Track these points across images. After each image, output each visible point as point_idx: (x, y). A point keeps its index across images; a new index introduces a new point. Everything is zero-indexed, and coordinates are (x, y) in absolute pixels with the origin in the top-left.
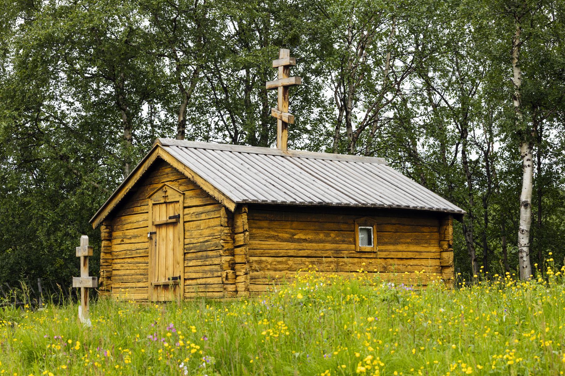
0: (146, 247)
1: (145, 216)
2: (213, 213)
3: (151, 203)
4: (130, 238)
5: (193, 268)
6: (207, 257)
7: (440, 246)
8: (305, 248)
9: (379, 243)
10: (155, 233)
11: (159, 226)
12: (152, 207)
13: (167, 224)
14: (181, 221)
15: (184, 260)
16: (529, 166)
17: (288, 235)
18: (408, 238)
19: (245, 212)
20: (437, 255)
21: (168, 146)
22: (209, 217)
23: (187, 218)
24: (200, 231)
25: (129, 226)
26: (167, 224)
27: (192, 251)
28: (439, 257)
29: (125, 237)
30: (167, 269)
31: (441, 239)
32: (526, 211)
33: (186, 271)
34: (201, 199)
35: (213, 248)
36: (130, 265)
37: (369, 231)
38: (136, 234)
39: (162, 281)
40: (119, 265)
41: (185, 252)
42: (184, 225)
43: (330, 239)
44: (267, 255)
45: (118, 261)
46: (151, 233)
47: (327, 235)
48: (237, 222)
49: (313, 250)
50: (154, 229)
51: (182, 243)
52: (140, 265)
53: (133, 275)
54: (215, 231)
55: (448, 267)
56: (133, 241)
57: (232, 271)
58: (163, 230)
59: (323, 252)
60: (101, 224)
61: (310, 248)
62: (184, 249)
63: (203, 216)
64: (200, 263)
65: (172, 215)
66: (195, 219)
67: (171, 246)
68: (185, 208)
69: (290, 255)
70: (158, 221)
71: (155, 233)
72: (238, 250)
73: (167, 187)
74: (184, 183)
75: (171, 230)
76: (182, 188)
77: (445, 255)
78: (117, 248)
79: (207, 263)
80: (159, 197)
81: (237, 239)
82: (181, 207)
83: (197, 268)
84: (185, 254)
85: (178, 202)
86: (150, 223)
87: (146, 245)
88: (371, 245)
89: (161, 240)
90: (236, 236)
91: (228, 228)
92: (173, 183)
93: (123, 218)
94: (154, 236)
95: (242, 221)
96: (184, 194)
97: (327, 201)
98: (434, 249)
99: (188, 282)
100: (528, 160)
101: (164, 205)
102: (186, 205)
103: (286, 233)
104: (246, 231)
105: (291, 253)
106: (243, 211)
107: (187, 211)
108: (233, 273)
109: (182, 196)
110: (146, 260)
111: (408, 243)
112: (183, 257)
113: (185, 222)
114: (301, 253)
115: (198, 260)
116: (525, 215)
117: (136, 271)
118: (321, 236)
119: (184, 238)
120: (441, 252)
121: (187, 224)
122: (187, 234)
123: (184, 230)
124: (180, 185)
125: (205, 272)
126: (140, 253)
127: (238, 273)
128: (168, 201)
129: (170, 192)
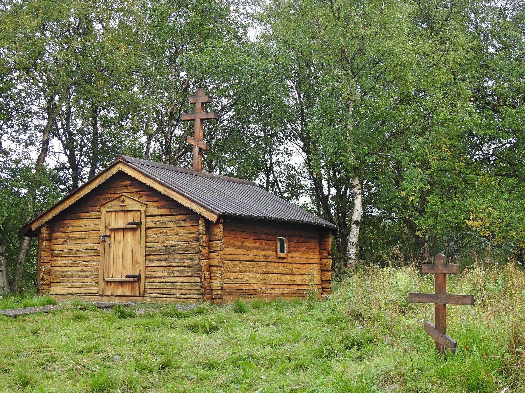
0: (96, 248)
1: (96, 221)
2: (183, 222)
3: (103, 210)
4: (76, 240)
5: (157, 268)
6: (174, 260)
7: (321, 254)
8: (249, 253)
9: (290, 251)
10: (109, 236)
11: (115, 230)
12: (106, 214)
13: (124, 230)
14: (143, 227)
15: (146, 261)
16: (360, 194)
17: (239, 243)
18: (303, 247)
19: (222, 223)
20: (317, 261)
21: (130, 163)
22: (178, 225)
23: (151, 225)
24: (166, 237)
25: (70, 229)
26: (124, 230)
27: (155, 253)
28: (319, 263)
29: (69, 238)
30: (124, 267)
31: (322, 248)
32: (357, 228)
33: (146, 271)
34: (167, 210)
35: (182, 252)
36: (74, 262)
37: (282, 242)
38: (83, 236)
39: (118, 278)
40: (60, 262)
41: (147, 254)
42: (146, 231)
43: (262, 246)
44: (228, 259)
45: (59, 259)
46: (105, 236)
47: (261, 244)
48: (213, 231)
49: (253, 255)
50: (108, 233)
51: (143, 246)
52: (87, 263)
53: (78, 271)
54: (185, 238)
55: (328, 271)
56: (78, 242)
57: (208, 273)
58: (120, 235)
59: (259, 257)
60: (43, 226)
61: (252, 254)
62: (146, 251)
63: (171, 224)
64: (165, 264)
65: (132, 221)
66: (159, 226)
67: (129, 248)
68: (147, 216)
69: (241, 259)
70: (113, 226)
71: (109, 236)
72: (213, 255)
73: (125, 198)
74: (146, 195)
75: (129, 236)
76: (142, 200)
77: (325, 261)
78: (58, 248)
79: (175, 264)
80: (115, 205)
81: (212, 246)
82: (143, 216)
83: (162, 269)
84: (146, 256)
85: (140, 211)
86: (102, 227)
87: (97, 246)
88: (284, 252)
89: (117, 243)
90: (211, 243)
91: (205, 236)
92: (132, 194)
93: (67, 222)
94: (107, 239)
95: (219, 230)
96: (146, 205)
97: (293, 218)
98: (315, 258)
99: (150, 280)
100: (359, 189)
101: (121, 214)
102: (148, 214)
103: (239, 241)
104: (222, 239)
105: (242, 258)
106: (221, 222)
107: (149, 219)
108: (209, 274)
109: (145, 207)
110: (96, 259)
111: (303, 251)
112: (144, 258)
113: (146, 228)
114: (248, 258)
115: (163, 262)
116: (355, 232)
117: (82, 268)
118: (257, 245)
119: (146, 242)
120: (321, 259)
121: (149, 231)
122: (149, 239)
123: (146, 235)
124: (142, 196)
125: (173, 272)
126: (87, 253)
127: (213, 274)
128: (125, 209)
129: (128, 202)
